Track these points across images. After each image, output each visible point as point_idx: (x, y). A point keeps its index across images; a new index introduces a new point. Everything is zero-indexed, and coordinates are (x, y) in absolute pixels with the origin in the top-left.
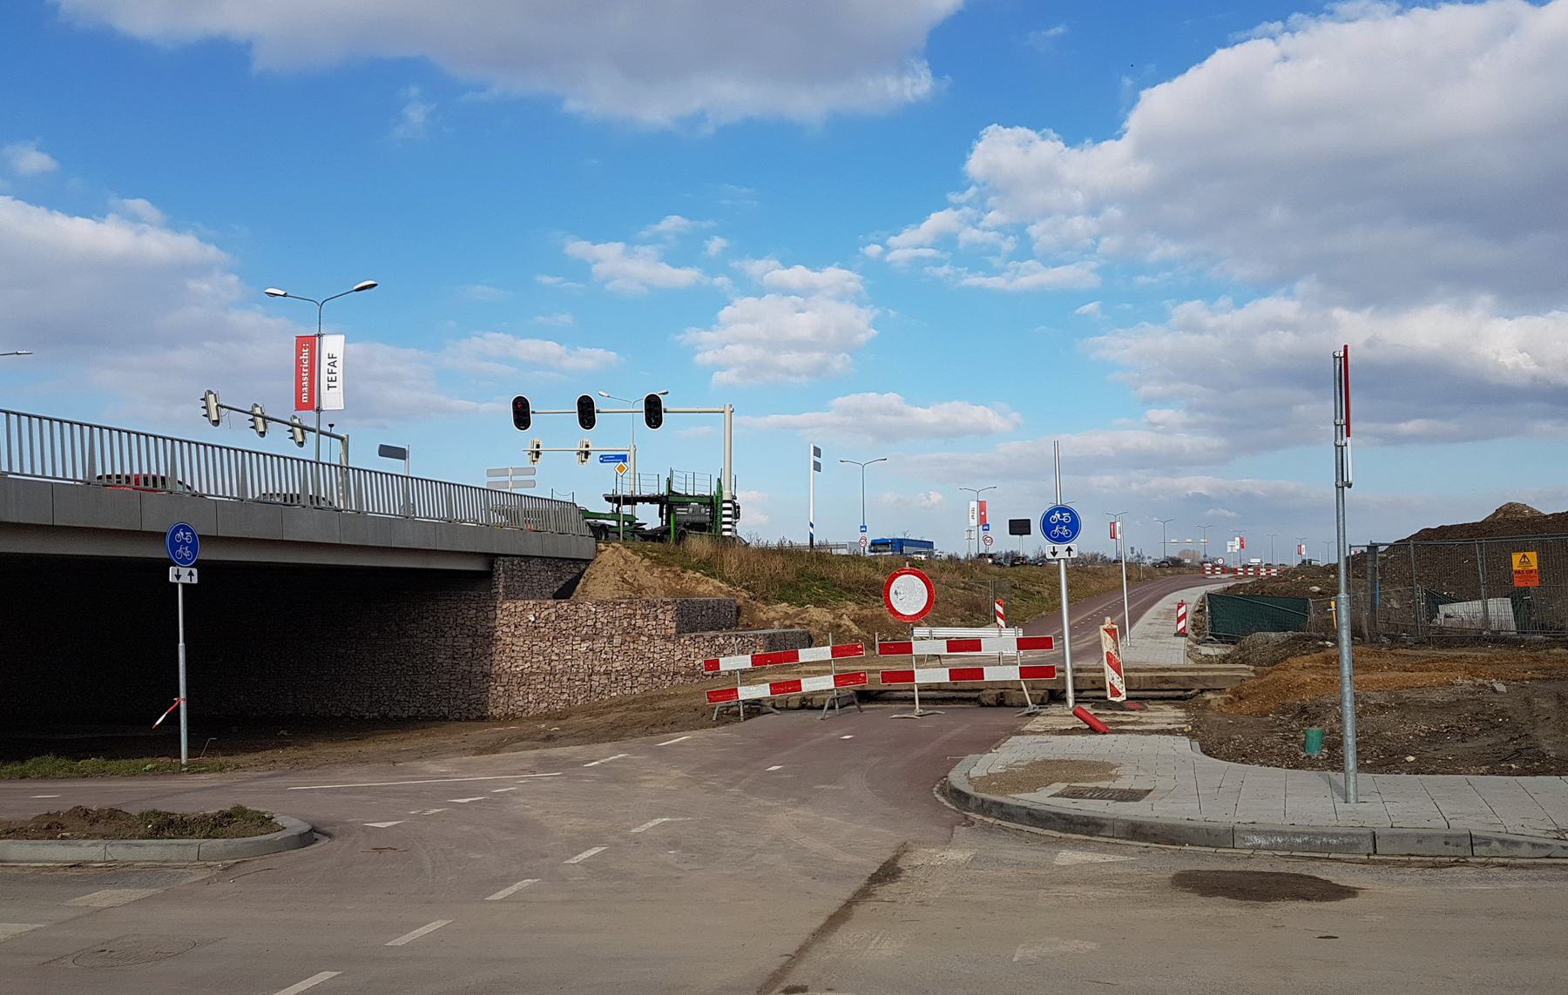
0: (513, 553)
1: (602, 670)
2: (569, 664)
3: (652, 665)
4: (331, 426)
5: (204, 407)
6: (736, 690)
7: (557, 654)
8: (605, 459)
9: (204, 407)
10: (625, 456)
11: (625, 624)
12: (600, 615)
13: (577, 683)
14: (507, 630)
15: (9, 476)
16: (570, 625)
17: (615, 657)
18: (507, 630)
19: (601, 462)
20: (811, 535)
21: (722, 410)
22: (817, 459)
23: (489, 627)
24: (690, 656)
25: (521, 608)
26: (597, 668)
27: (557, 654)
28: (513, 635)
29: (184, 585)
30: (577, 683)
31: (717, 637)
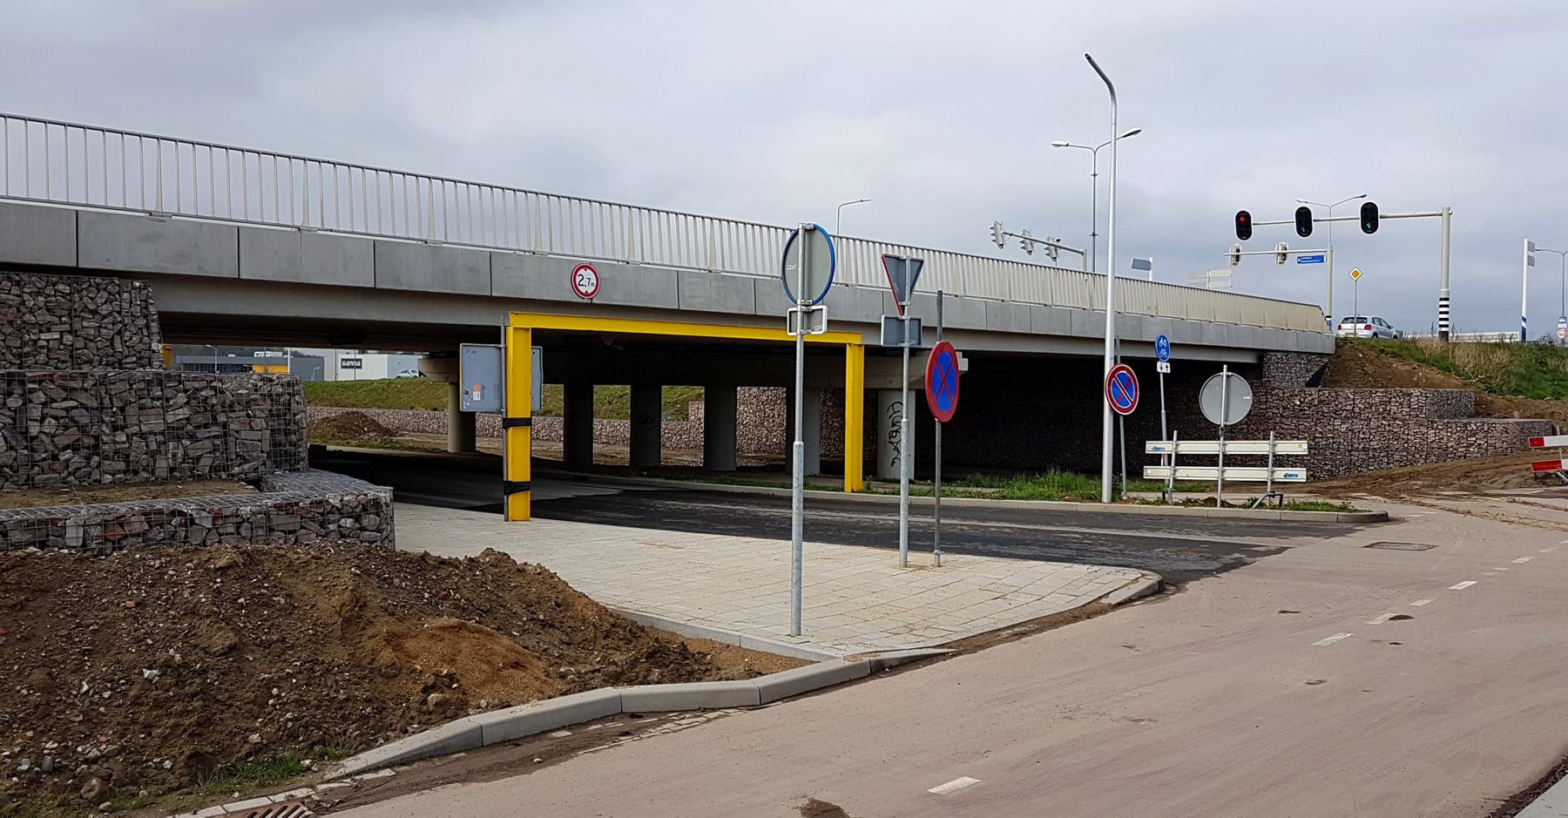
0: (1275, 348)
1: (1361, 447)
2: (1331, 440)
3: (1406, 445)
4: (1058, 241)
5: (993, 235)
6: (1560, 462)
7: (1320, 433)
8: (1301, 260)
9: (993, 235)
10: (1323, 257)
11: (1381, 410)
12: (1358, 401)
13: (1338, 457)
14: (1276, 411)
15: (549, 256)
16: (1331, 409)
17: (1372, 437)
18: (1276, 411)
19: (1299, 263)
20: (1524, 329)
21: (1440, 212)
22: (1531, 254)
23: (1261, 409)
24: (1442, 439)
25: (1289, 394)
26: (1356, 446)
27: (1320, 433)
28: (1281, 415)
29: (1164, 374)
30: (1338, 457)
31: (1470, 423)
